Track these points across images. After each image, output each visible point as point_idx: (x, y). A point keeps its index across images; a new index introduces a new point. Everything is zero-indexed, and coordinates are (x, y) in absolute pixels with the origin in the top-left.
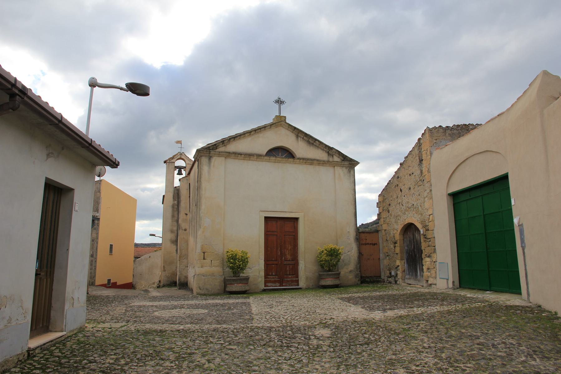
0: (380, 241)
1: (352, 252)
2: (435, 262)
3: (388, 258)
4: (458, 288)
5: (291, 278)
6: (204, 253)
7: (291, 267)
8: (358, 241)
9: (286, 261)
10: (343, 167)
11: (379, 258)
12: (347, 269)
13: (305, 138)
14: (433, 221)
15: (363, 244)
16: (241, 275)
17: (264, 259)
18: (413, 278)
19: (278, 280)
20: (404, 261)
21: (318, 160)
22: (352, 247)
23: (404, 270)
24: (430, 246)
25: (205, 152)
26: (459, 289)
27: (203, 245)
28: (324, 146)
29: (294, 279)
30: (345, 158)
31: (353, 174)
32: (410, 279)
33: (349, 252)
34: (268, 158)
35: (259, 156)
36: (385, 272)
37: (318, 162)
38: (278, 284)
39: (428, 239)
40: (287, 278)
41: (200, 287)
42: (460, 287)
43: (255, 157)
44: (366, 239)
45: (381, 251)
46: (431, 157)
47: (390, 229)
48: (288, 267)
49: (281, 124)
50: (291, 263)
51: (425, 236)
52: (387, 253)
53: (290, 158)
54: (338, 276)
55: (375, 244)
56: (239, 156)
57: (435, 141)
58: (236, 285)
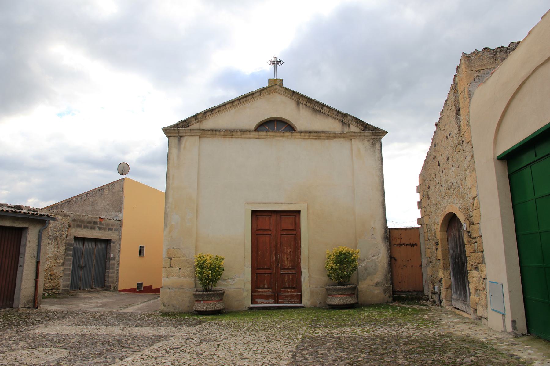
0: (422, 241)
2: (484, 279)
4: (523, 335)
5: (291, 292)
6: (171, 259)
7: (291, 277)
8: (388, 241)
10: (364, 139)
11: (421, 265)
12: (372, 280)
13: (308, 104)
14: (478, 207)
15: (397, 245)
16: (214, 288)
17: (250, 267)
18: (461, 300)
19: (272, 295)
20: (449, 271)
21: (326, 133)
23: (450, 285)
24: (476, 251)
25: (172, 131)
26: (525, 338)
27: (169, 249)
28: (336, 113)
29: (296, 294)
30: (366, 127)
31: (379, 148)
32: (457, 300)
33: (374, 256)
34: (256, 133)
35: (243, 131)
36: (429, 285)
37: (327, 135)
38: (271, 301)
39: (474, 238)
40: (285, 292)
41: (164, 303)
42: (529, 332)
43: (239, 133)
44: (401, 238)
46: (470, 100)
47: (431, 223)
48: (286, 277)
49: (275, 90)
50: (291, 271)
51: (469, 234)
52: (430, 258)
54: (354, 291)
55: (413, 245)
56: (218, 133)
57: (476, 74)
58: (202, 302)
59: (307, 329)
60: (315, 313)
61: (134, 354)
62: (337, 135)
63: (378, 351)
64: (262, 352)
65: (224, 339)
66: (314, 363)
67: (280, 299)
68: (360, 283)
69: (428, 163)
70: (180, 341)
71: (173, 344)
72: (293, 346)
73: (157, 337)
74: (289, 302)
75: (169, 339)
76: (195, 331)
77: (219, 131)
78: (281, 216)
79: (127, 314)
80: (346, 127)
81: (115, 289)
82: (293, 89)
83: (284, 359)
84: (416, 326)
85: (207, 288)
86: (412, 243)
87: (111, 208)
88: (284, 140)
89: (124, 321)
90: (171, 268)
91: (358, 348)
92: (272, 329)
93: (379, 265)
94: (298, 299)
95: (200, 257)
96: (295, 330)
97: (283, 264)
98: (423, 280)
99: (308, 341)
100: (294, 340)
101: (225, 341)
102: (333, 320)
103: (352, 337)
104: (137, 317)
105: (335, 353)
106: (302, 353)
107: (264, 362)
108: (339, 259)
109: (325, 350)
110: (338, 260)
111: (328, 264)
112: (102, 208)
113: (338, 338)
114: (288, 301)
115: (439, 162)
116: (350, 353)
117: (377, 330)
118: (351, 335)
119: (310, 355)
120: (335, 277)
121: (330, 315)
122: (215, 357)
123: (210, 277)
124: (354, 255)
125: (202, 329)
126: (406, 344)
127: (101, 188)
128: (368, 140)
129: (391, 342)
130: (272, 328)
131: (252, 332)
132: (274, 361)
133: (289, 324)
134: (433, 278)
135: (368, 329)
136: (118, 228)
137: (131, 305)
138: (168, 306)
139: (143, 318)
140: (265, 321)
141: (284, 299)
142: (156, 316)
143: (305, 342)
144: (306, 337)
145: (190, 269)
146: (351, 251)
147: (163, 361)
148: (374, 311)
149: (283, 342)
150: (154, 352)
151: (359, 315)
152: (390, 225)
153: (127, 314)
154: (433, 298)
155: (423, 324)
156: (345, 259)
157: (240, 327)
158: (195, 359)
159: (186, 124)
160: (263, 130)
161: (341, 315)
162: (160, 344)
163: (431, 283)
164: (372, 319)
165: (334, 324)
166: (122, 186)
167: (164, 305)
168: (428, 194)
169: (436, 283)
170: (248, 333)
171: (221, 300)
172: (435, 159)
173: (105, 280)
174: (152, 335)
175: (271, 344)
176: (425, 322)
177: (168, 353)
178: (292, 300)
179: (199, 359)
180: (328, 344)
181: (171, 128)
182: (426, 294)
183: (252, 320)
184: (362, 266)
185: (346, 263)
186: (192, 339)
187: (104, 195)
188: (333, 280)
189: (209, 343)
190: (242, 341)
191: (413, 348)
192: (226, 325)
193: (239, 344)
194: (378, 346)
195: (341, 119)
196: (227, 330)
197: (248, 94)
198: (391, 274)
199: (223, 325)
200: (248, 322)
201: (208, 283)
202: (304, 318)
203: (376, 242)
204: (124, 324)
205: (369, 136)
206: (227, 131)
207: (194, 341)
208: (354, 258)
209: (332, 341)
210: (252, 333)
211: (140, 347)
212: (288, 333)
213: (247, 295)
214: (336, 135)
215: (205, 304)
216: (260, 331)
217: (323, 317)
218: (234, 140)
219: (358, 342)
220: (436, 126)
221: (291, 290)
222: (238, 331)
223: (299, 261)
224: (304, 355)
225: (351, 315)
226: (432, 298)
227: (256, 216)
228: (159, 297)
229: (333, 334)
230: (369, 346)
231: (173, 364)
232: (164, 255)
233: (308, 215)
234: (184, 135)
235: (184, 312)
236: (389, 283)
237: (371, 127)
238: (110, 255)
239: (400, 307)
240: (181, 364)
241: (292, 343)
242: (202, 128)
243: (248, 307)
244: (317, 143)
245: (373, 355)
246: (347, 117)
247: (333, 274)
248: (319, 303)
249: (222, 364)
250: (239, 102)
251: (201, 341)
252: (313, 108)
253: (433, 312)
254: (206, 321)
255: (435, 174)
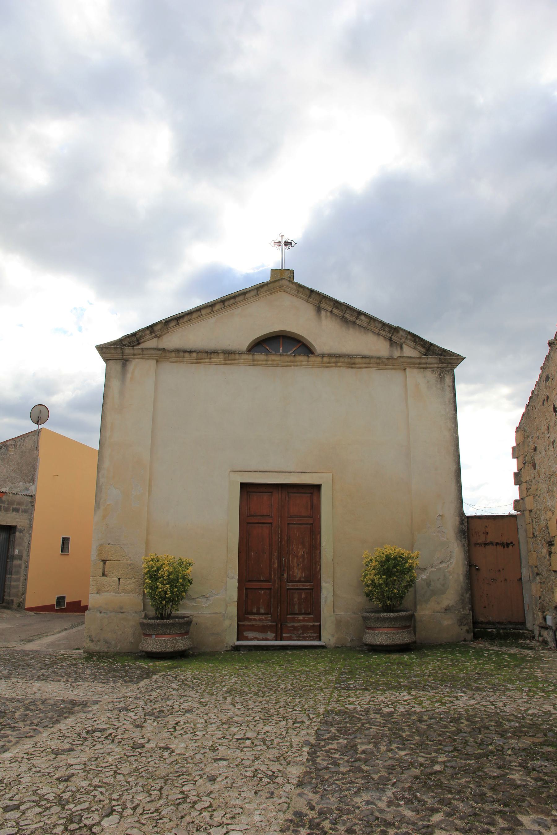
1: (451, 563)
3: (538, 579)
5: (304, 620)
6: (104, 561)
7: (303, 596)
8: (465, 538)
9: (292, 581)
10: (425, 368)
11: (521, 579)
12: (438, 603)
13: (335, 311)
15: (480, 544)
16: (174, 613)
19: (271, 626)
21: (363, 357)
22: (451, 552)
25: (113, 351)
27: (101, 545)
28: (380, 326)
29: (311, 624)
33: (442, 562)
34: (250, 357)
36: (534, 614)
37: (364, 360)
38: (271, 635)
40: (293, 620)
41: (90, 636)
43: (221, 356)
44: (487, 533)
45: (524, 562)
49: (281, 287)
50: (304, 586)
52: (536, 567)
53: (299, 355)
55: (508, 545)
56: (187, 355)
58: (154, 636)
59: (333, 692)
60: (344, 659)
61: (21, 742)
62: (382, 361)
63: (468, 748)
64: (253, 743)
65: (188, 711)
66: (351, 774)
67: (285, 633)
68: (418, 607)
69: (534, 408)
70: (108, 714)
71: (95, 721)
72: (309, 731)
73: (68, 705)
74: (301, 639)
75: (90, 709)
76: (138, 691)
77: (188, 352)
78: (288, 493)
79: (28, 655)
80: (397, 348)
81: (21, 606)
82: (310, 287)
83: (294, 762)
84: (525, 692)
85: (164, 612)
86: (505, 542)
87: (18, 476)
88: (296, 368)
89: (20, 670)
90: (105, 578)
91: (431, 741)
92: (271, 692)
93: (451, 577)
94: (314, 633)
95: (152, 560)
96: (312, 695)
97: (291, 573)
98: (524, 604)
99: (336, 720)
100: (311, 716)
101: (187, 715)
102: (377, 674)
103: (415, 712)
104: (44, 661)
105: (389, 751)
106: (327, 748)
107: (256, 770)
108: (385, 567)
109: (369, 743)
110: (384, 569)
111: (365, 575)
112: (4, 475)
113: (390, 714)
114: (299, 637)
115: (556, 406)
116: (417, 753)
117: (458, 700)
118: (413, 709)
119: (341, 755)
120: (377, 598)
121: (371, 664)
122: (166, 754)
123: (167, 594)
124: (410, 561)
125: (150, 688)
126: (518, 733)
127: (4, 444)
128: (433, 371)
129: (488, 728)
130: (271, 690)
131: (236, 696)
132: (275, 767)
133: (301, 680)
134: (543, 601)
135: (441, 697)
136: (27, 508)
137: (41, 635)
138: (98, 641)
139: (53, 663)
140: (260, 673)
141: (292, 633)
142: (75, 659)
143: (331, 722)
144: (332, 711)
145: (136, 579)
146: (406, 555)
147: (69, 762)
148: (446, 657)
149: (291, 721)
150: (56, 738)
151: (420, 665)
152: (469, 511)
153: (28, 655)
154: (542, 636)
155: (537, 688)
156: (395, 567)
157: (216, 686)
158: (129, 759)
159: (135, 339)
160: (261, 352)
161: (389, 664)
162: (71, 720)
163: (539, 609)
164: (445, 673)
165: (379, 684)
166: (36, 441)
167: (90, 640)
168: (533, 460)
169: (548, 610)
170: (229, 699)
171: (187, 633)
172: (547, 401)
173: (5, 592)
174: (61, 699)
175: (270, 724)
176: (540, 685)
177: (81, 743)
178: (305, 635)
179: (136, 758)
180: (374, 729)
181: (111, 345)
182: (530, 629)
183: (237, 672)
184: (422, 579)
185: (396, 574)
186: (130, 709)
187: (8, 456)
188: (375, 602)
189: (159, 719)
190: (218, 717)
191: (534, 744)
192: (192, 681)
193: (212, 724)
194: (466, 737)
195: (388, 335)
196: (192, 693)
197: (237, 293)
198: (470, 593)
199: (186, 680)
200: (231, 675)
201: (165, 605)
202: (327, 669)
203: (445, 539)
204: (18, 675)
205: (435, 364)
206: (203, 352)
207: (132, 714)
208: (410, 566)
209: (380, 722)
210: (236, 698)
211: (35, 727)
212: (299, 700)
213: (231, 625)
214: (381, 362)
215: (158, 640)
216: (251, 695)
217: (358, 668)
218: (212, 367)
219: (427, 725)
220: (549, 346)
221: (303, 617)
222: (212, 694)
223: (318, 569)
224: (331, 753)
225: (406, 665)
226: (540, 635)
227: (248, 492)
228: (83, 623)
229: (380, 705)
230: (450, 737)
231: (86, 770)
232: (94, 555)
233: (333, 492)
234: (131, 358)
235: (124, 653)
236: (467, 608)
237: (438, 350)
238: (14, 551)
239: (489, 651)
240: (101, 771)
241: (307, 723)
242: (161, 346)
243: (232, 646)
244: (348, 375)
245: (461, 759)
246: (398, 332)
247: (375, 592)
248: (351, 641)
249: (178, 772)
250: (223, 306)
251: (145, 715)
252: (343, 317)
253: (548, 662)
254: (159, 671)
255: (548, 427)
